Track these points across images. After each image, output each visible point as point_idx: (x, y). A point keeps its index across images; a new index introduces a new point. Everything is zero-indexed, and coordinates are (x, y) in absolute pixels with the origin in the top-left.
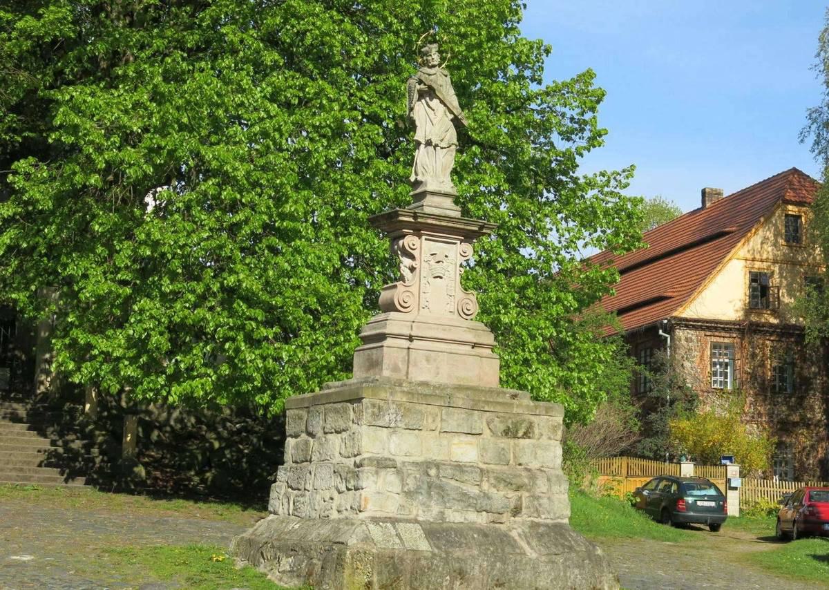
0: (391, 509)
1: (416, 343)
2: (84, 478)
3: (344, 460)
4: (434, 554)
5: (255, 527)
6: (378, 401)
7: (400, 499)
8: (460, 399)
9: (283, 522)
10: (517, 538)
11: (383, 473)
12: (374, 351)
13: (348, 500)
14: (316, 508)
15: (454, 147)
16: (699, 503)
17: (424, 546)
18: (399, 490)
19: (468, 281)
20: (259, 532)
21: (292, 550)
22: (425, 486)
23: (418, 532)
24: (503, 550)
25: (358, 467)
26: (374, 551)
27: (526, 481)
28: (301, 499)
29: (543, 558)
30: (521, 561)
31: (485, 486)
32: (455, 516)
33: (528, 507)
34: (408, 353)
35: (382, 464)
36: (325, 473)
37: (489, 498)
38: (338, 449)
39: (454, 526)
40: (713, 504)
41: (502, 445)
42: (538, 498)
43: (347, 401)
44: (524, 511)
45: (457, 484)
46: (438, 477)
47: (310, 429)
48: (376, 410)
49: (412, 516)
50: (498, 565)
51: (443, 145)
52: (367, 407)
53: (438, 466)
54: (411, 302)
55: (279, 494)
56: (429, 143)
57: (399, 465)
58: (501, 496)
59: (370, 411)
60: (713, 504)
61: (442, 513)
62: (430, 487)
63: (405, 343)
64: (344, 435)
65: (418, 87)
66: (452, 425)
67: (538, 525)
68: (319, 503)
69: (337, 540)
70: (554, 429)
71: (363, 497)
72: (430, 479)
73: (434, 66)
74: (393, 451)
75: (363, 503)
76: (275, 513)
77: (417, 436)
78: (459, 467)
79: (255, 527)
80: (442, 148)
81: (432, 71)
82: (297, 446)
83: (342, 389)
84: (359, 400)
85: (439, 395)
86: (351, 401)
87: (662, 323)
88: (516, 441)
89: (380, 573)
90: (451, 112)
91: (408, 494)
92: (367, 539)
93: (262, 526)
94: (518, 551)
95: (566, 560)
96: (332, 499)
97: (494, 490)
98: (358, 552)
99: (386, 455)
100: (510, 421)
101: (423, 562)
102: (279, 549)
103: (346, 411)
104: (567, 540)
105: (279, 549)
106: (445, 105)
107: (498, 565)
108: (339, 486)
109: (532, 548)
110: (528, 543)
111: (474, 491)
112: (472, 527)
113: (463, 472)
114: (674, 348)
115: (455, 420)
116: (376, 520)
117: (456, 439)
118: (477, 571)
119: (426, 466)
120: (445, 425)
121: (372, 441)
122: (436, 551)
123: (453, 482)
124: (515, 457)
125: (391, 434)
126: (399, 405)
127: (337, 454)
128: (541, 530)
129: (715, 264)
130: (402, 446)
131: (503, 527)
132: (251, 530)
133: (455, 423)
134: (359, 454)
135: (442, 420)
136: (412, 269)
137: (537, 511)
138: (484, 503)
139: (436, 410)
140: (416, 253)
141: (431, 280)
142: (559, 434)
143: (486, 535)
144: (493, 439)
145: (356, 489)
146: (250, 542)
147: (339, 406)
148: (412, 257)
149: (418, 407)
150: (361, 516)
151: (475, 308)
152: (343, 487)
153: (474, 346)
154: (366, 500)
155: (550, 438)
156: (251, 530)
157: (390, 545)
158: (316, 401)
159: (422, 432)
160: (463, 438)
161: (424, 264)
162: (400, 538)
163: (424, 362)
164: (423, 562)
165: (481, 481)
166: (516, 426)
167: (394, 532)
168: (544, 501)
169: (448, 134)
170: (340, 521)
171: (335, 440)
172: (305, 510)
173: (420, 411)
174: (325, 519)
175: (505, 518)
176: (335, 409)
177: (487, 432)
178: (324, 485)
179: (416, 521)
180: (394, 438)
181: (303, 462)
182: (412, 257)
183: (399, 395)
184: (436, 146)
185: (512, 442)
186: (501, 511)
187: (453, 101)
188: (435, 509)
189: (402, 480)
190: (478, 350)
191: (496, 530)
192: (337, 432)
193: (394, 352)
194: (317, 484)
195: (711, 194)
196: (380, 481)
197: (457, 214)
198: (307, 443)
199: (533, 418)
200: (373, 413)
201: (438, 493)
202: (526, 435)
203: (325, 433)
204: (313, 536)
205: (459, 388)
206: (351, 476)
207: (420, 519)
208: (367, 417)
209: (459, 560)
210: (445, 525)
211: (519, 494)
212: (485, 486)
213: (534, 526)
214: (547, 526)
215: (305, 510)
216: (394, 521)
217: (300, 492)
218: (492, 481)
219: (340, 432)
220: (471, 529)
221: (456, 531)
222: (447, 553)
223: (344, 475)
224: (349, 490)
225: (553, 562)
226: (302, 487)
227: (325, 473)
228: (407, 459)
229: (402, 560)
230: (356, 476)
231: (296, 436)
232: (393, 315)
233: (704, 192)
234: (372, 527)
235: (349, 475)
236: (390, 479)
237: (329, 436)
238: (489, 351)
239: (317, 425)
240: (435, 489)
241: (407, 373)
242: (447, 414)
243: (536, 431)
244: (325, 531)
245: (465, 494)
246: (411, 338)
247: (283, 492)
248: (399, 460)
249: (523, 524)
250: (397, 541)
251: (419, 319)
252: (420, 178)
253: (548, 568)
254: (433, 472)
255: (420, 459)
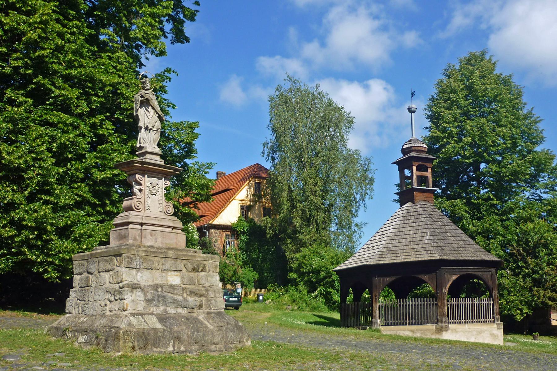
0: (140, 308)
1: (144, 227)
2: (340, 319)
3: (111, 285)
4: (164, 330)
5: (59, 321)
6: (130, 255)
7: (143, 304)
8: (171, 254)
9: (76, 317)
10: (202, 319)
11: (135, 291)
12: (123, 231)
13: (115, 306)
14: (97, 309)
15: (159, 130)
16: (231, 299)
17: (159, 326)
18: (143, 299)
19: (168, 197)
20: (62, 323)
21: (85, 332)
22: (157, 297)
23: (155, 319)
24: (197, 326)
25: (121, 288)
26: (135, 330)
27: (204, 292)
28: (87, 306)
29: (216, 329)
30: (206, 331)
31: (185, 295)
32: (171, 311)
33: (205, 305)
34: (141, 232)
35: (134, 287)
36: (101, 292)
37: (187, 301)
38: (107, 279)
39: (172, 316)
40: (236, 299)
41: (192, 276)
42: (210, 300)
43: (112, 256)
44: (204, 306)
45: (172, 295)
46: (162, 292)
47: (90, 270)
48: (129, 260)
49: (151, 312)
50: (196, 333)
51: (154, 129)
52: (125, 259)
53: (162, 286)
54: (141, 207)
55: (71, 303)
56: (147, 128)
57: (142, 287)
58: (192, 300)
59: (126, 260)
60: (236, 299)
61: (165, 309)
62: (159, 297)
63: (139, 227)
64: (111, 273)
65: (141, 99)
66: (167, 266)
67: (211, 313)
68: (98, 307)
69: (113, 326)
70: (215, 267)
71: (125, 304)
72: (158, 294)
73: (148, 90)
74: (139, 280)
75: (125, 306)
76: (70, 313)
77: (151, 273)
78: (172, 287)
79: (59, 321)
80: (153, 131)
81: (147, 92)
82: (81, 279)
83: (106, 250)
84: (120, 255)
85: (153, 252)
86: (115, 256)
87: (204, 226)
88: (198, 273)
89: (138, 341)
90: (157, 113)
91: (148, 301)
92: (130, 324)
93: (61, 320)
94: (204, 326)
95: (226, 329)
96: (106, 305)
97: (189, 298)
98: (127, 331)
99: (135, 282)
100: (195, 264)
101: (160, 334)
102: (76, 331)
103: (111, 260)
104: (225, 319)
105: (76, 331)
106: (154, 110)
107: (196, 333)
108: (110, 298)
109: (210, 324)
110: (208, 322)
111: (180, 298)
112: (180, 315)
113: (174, 289)
114: (209, 236)
115: (169, 264)
116: (133, 315)
117: (170, 273)
118: (185, 337)
119: (156, 287)
120: (164, 266)
121: (128, 276)
122: (165, 328)
123: (170, 295)
124: (198, 281)
125: (137, 272)
126: (141, 257)
127: (107, 282)
128: (212, 315)
129: (227, 202)
130: (142, 277)
131: (195, 315)
132: (57, 323)
133: (169, 266)
134: (121, 282)
135: (162, 264)
136: (140, 190)
137: (210, 306)
138: (185, 303)
139: (159, 259)
140: (142, 182)
141: (150, 196)
142: (218, 270)
143: (187, 319)
144: (187, 273)
145: (121, 300)
146: (57, 328)
147: (107, 258)
148: (140, 184)
149: (151, 258)
150: (125, 313)
151: (172, 210)
152: (112, 299)
153: (173, 228)
154: (127, 305)
155: (213, 272)
156: (57, 323)
157: (142, 327)
158: (92, 256)
159: (153, 271)
160: (173, 273)
161: (147, 188)
162: (147, 323)
163: (150, 236)
164: (160, 334)
165: (183, 293)
166: (198, 266)
167: (143, 320)
168: (213, 302)
169: (157, 123)
170: (112, 316)
171: (106, 276)
172: (90, 311)
173: (152, 260)
174: (103, 315)
175: (195, 311)
176: (105, 260)
177: (184, 270)
178: (100, 298)
179: (152, 314)
180: (139, 273)
181: (85, 287)
182: (140, 184)
183: (141, 252)
184: (151, 129)
185: (196, 274)
186: (193, 307)
187: (158, 108)
188: (162, 308)
189: (145, 294)
190: (175, 231)
191: (192, 317)
192: (107, 271)
193: (134, 231)
194: (96, 298)
195: (221, 174)
196: (134, 296)
197: (163, 163)
198: (88, 278)
199: (205, 262)
200: (128, 261)
201: (163, 300)
202: (203, 271)
203: (99, 272)
204: (97, 324)
205: (169, 249)
206: (117, 294)
207: (155, 313)
208: (125, 263)
209: (177, 332)
210: (167, 315)
211: (201, 298)
212: (185, 295)
213: (209, 313)
214: (214, 313)
215: (90, 311)
216: (142, 315)
217: (85, 302)
218: (188, 293)
219: (108, 271)
220: (179, 316)
221: (173, 318)
222: (171, 329)
223: (112, 293)
224: (116, 300)
225: (221, 330)
226: (86, 299)
227: (101, 292)
228: (146, 284)
229: (149, 334)
230: (120, 293)
231: (81, 274)
232: (132, 212)
233: (217, 173)
234: (131, 318)
235: (116, 293)
236: (139, 295)
237: (101, 274)
238: (180, 231)
239: (93, 268)
240: (162, 299)
241: (141, 241)
242: (165, 261)
243: (207, 268)
244: (104, 321)
245: (176, 300)
246: (142, 224)
247: (74, 302)
248: (142, 284)
249: (204, 313)
250: (146, 324)
251: (145, 215)
252: (142, 145)
253: (219, 333)
254: (160, 290)
255: (152, 284)
